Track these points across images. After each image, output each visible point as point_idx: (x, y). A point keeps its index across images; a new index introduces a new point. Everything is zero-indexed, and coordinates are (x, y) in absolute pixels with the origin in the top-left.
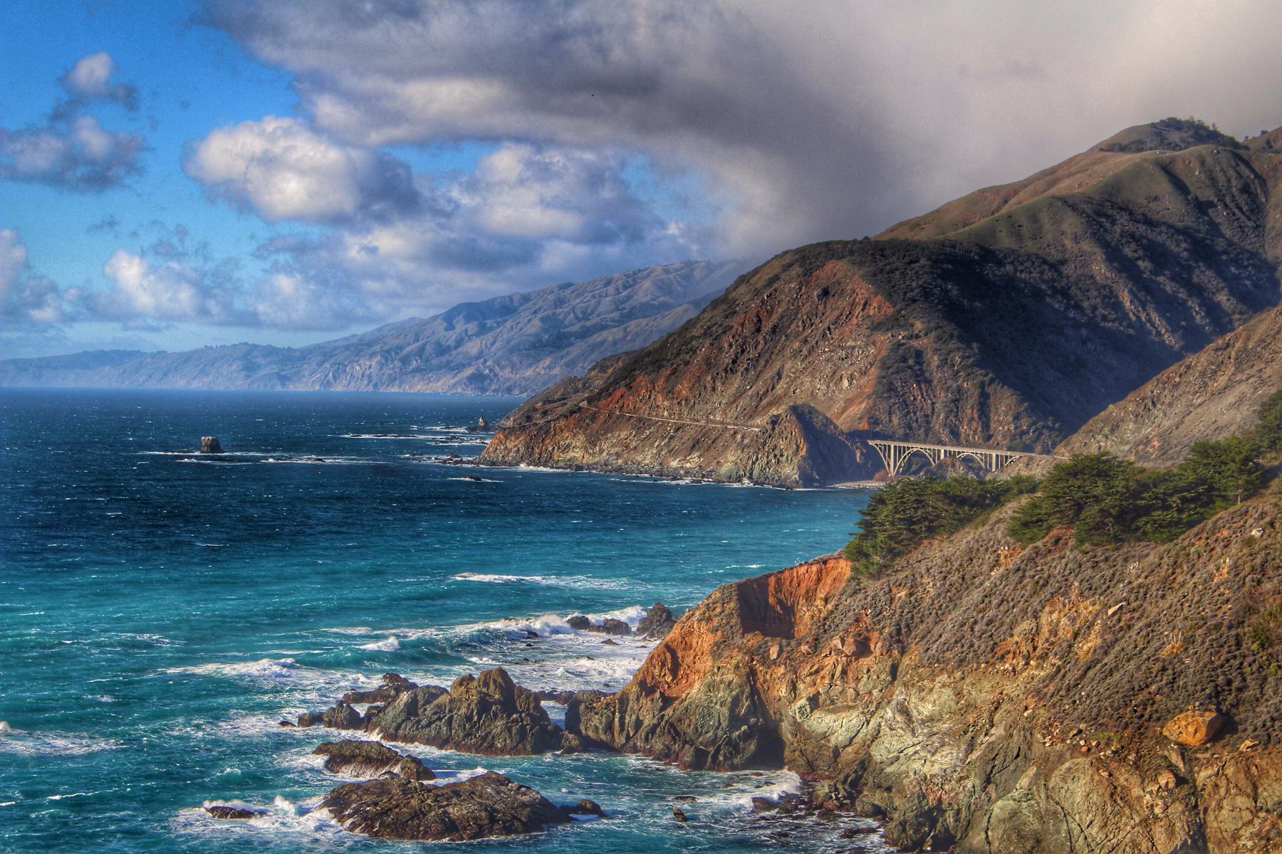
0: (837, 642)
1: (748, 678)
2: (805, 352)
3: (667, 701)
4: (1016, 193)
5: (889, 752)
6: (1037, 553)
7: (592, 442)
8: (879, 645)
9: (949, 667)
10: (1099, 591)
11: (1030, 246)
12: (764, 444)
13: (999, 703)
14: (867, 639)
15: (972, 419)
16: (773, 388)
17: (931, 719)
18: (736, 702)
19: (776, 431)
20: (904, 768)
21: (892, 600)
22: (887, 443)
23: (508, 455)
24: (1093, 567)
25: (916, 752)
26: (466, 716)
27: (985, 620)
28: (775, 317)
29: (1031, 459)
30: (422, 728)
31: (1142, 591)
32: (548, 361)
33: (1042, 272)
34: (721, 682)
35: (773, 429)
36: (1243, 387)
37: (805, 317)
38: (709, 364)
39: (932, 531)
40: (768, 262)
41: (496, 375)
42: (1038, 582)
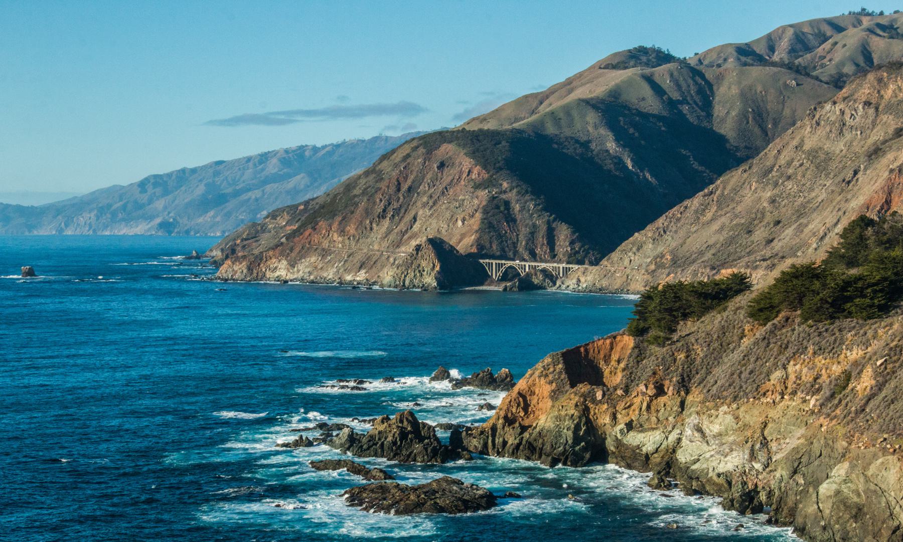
0: (642, 387)
1: (584, 412)
2: (431, 203)
3: (524, 429)
4: (547, 97)
5: (692, 456)
6: (775, 328)
7: (292, 265)
8: (671, 388)
9: (727, 401)
10: (827, 351)
11: (567, 132)
12: (412, 263)
13: (766, 424)
14: (662, 386)
15: (543, 244)
16: (411, 227)
17: (720, 434)
18: (577, 428)
19: (419, 255)
20: (705, 466)
21: (675, 360)
22: (491, 261)
23: (235, 274)
24: (819, 336)
25: (712, 456)
26: (393, 442)
27: (748, 371)
28: (409, 182)
29: (586, 269)
30: (365, 450)
31: (898, 349)
32: (211, 213)
33: (575, 149)
34: (566, 415)
35: (417, 254)
36: (723, 219)
37: (429, 181)
38: (367, 212)
39: (685, 316)
40: (401, 146)
41: (178, 222)
42: (781, 346)
